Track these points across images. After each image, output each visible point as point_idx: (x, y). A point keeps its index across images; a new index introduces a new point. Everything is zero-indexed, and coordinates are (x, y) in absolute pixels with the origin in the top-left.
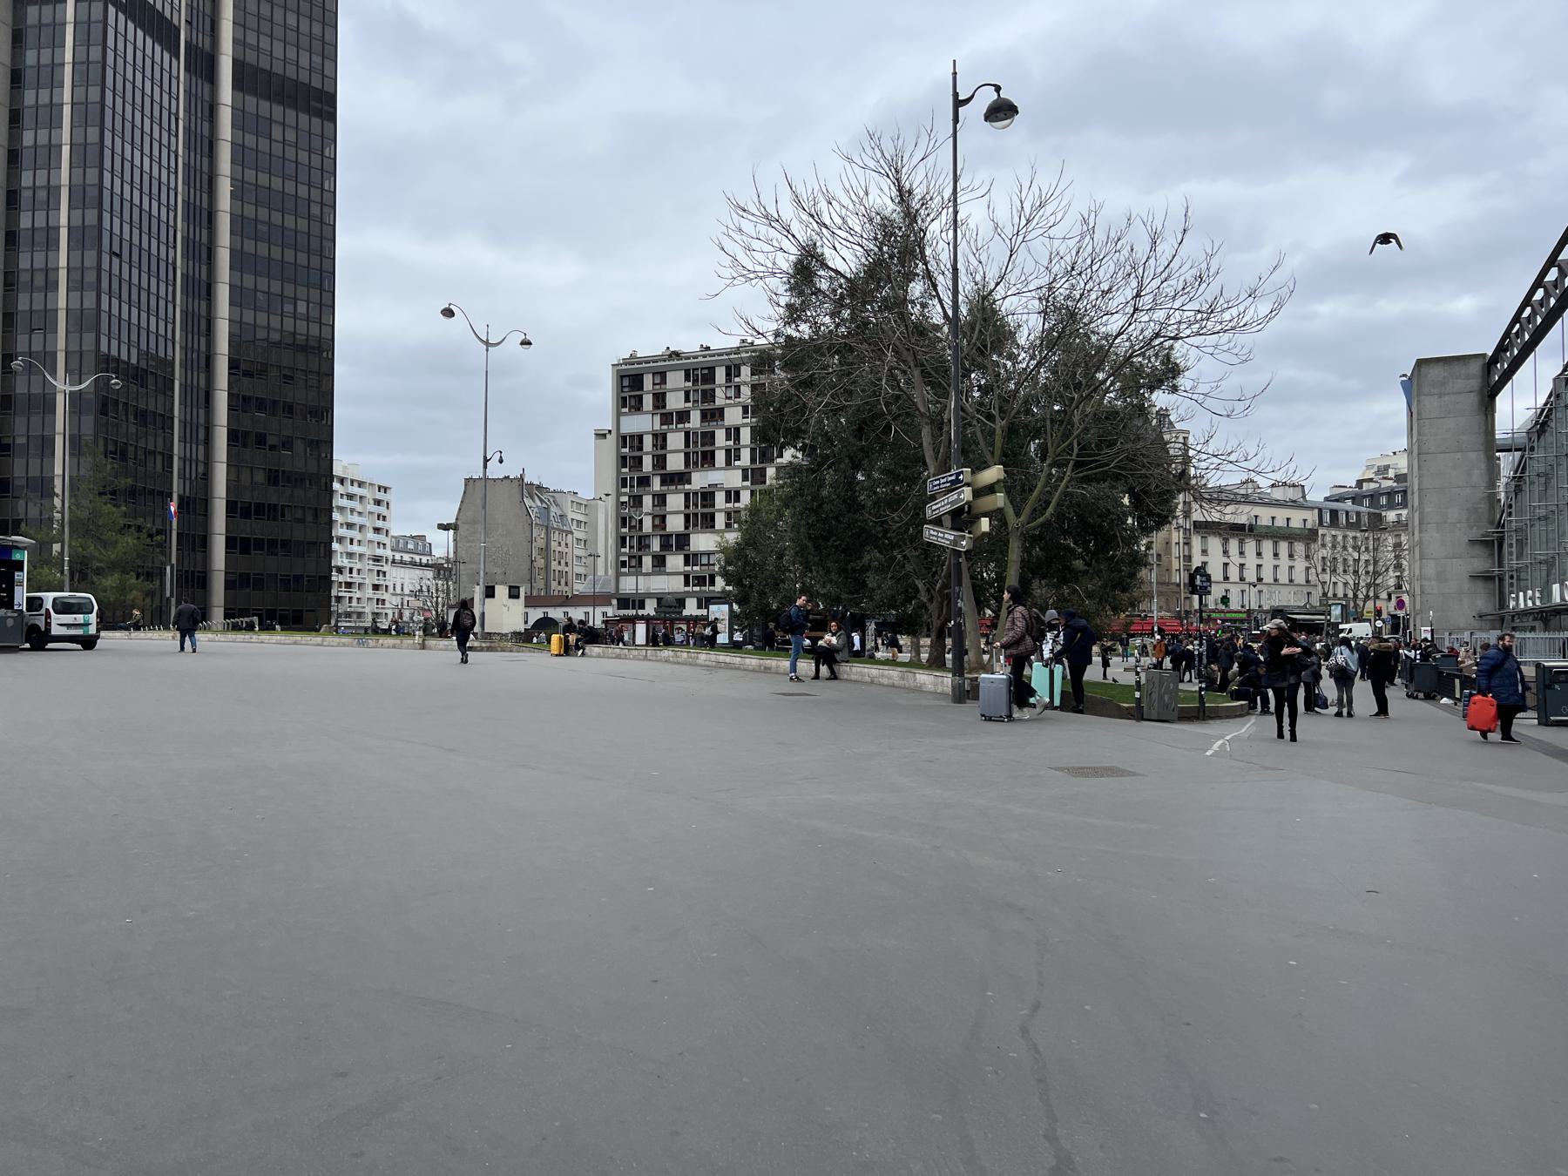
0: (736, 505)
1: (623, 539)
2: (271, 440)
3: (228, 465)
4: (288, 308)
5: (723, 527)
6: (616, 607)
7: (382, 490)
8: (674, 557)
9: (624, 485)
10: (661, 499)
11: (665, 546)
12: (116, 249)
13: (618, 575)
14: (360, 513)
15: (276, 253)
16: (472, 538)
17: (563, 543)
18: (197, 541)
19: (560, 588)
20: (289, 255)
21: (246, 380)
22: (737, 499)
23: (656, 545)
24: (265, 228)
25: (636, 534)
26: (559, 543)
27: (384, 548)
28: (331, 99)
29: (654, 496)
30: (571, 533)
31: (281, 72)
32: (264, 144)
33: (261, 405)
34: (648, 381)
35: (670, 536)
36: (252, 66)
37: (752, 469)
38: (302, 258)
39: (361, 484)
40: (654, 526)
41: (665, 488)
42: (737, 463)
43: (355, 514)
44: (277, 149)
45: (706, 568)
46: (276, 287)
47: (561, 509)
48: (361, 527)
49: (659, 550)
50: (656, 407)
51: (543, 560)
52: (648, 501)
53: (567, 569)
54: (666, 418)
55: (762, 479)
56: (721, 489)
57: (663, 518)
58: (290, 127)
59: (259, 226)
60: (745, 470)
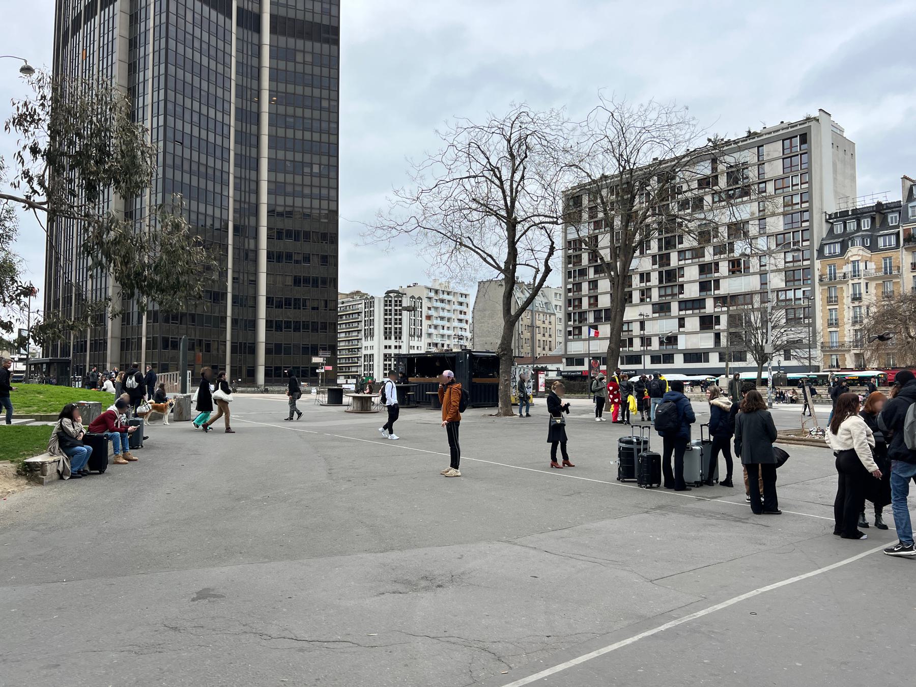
0: (648, 284)
1: (569, 315)
2: (295, 257)
3: (267, 274)
4: (307, 170)
5: (638, 301)
6: (565, 364)
7: (464, 296)
8: (603, 326)
9: (570, 277)
10: (594, 284)
11: (598, 319)
12: (179, 138)
13: (566, 341)
14: (449, 311)
15: (299, 135)
16: (482, 321)
17: (547, 322)
18: (247, 324)
19: (544, 352)
20: (308, 135)
21: (279, 219)
22: (649, 280)
23: (591, 318)
24: (292, 120)
25: (577, 311)
26: (544, 322)
27: (465, 331)
28: (336, 30)
29: (589, 282)
30: (554, 314)
31: (293, 16)
32: (291, 67)
33: (289, 234)
34: (585, 201)
35: (601, 310)
36: (282, 17)
37: (659, 255)
38: (316, 137)
39: (448, 293)
40: (590, 304)
41: (597, 276)
42: (648, 252)
43: (445, 311)
44: (300, 68)
45: (627, 333)
46: (299, 157)
47: (548, 299)
48: (449, 320)
49: (593, 321)
50: (591, 217)
51: (529, 334)
52: (585, 286)
53: (550, 339)
54: (597, 225)
55: (668, 262)
56: (636, 273)
57: (596, 298)
58: (308, 52)
59: (288, 119)
60: (654, 257)
